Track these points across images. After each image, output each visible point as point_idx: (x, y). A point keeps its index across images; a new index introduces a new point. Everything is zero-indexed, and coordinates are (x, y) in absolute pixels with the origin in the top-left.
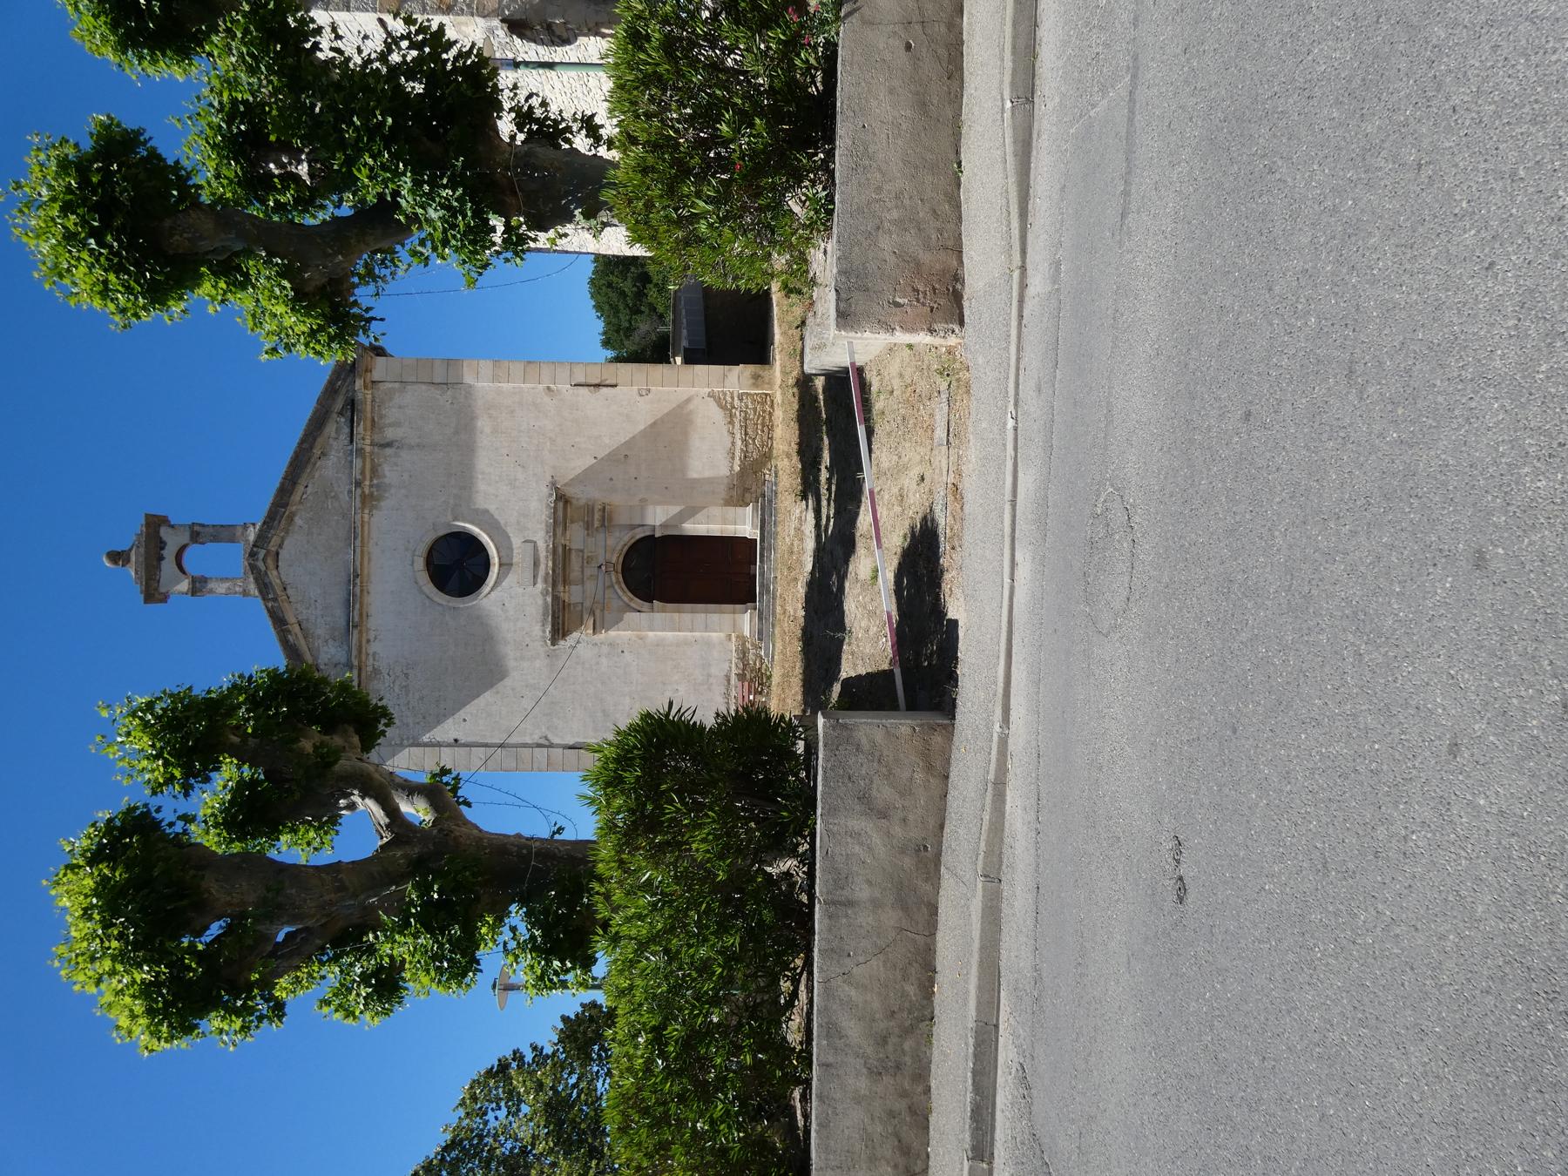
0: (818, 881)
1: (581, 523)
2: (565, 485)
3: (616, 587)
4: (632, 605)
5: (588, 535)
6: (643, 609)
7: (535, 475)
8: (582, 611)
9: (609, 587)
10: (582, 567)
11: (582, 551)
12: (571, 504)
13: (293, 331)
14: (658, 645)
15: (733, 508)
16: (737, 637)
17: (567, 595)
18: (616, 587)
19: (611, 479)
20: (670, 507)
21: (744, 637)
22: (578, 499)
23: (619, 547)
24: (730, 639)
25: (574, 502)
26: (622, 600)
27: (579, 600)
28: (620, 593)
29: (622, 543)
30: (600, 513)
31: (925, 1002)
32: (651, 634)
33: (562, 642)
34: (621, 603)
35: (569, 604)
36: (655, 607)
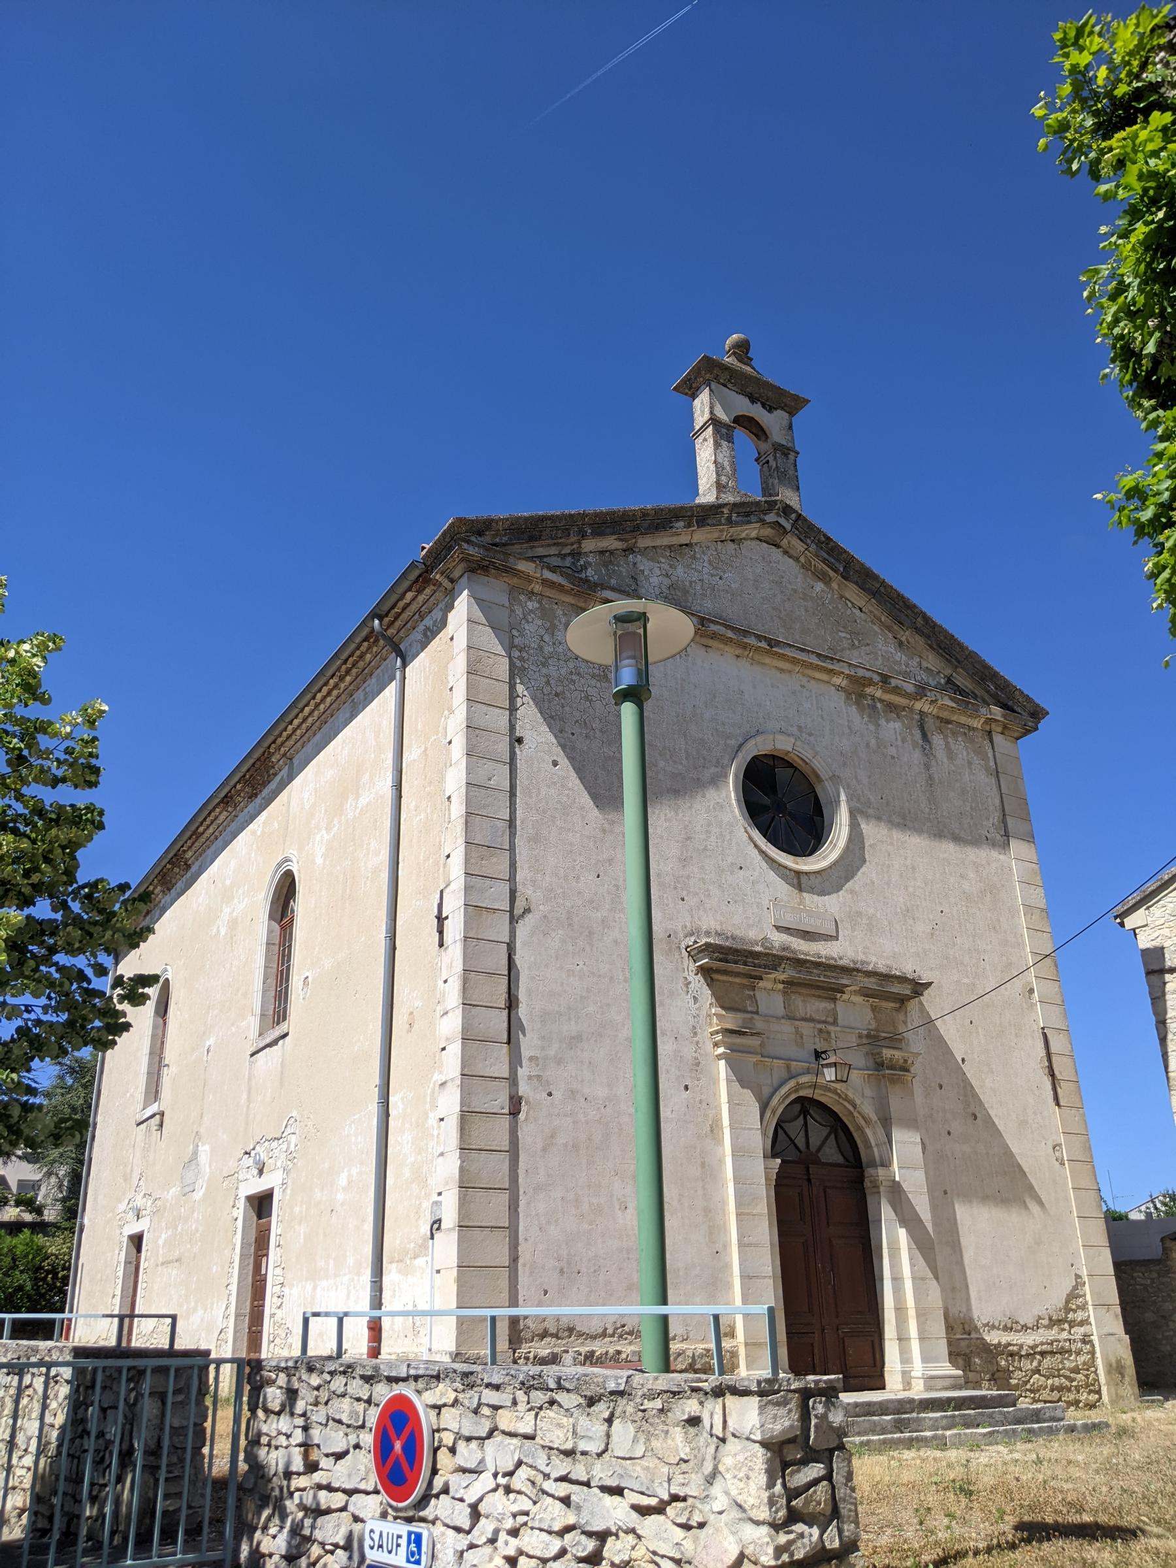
3: (792, 1083)
5: (860, 1036)
12: (898, 1010)
14: (703, 1165)
29: (858, 1102)
35: (753, 988)
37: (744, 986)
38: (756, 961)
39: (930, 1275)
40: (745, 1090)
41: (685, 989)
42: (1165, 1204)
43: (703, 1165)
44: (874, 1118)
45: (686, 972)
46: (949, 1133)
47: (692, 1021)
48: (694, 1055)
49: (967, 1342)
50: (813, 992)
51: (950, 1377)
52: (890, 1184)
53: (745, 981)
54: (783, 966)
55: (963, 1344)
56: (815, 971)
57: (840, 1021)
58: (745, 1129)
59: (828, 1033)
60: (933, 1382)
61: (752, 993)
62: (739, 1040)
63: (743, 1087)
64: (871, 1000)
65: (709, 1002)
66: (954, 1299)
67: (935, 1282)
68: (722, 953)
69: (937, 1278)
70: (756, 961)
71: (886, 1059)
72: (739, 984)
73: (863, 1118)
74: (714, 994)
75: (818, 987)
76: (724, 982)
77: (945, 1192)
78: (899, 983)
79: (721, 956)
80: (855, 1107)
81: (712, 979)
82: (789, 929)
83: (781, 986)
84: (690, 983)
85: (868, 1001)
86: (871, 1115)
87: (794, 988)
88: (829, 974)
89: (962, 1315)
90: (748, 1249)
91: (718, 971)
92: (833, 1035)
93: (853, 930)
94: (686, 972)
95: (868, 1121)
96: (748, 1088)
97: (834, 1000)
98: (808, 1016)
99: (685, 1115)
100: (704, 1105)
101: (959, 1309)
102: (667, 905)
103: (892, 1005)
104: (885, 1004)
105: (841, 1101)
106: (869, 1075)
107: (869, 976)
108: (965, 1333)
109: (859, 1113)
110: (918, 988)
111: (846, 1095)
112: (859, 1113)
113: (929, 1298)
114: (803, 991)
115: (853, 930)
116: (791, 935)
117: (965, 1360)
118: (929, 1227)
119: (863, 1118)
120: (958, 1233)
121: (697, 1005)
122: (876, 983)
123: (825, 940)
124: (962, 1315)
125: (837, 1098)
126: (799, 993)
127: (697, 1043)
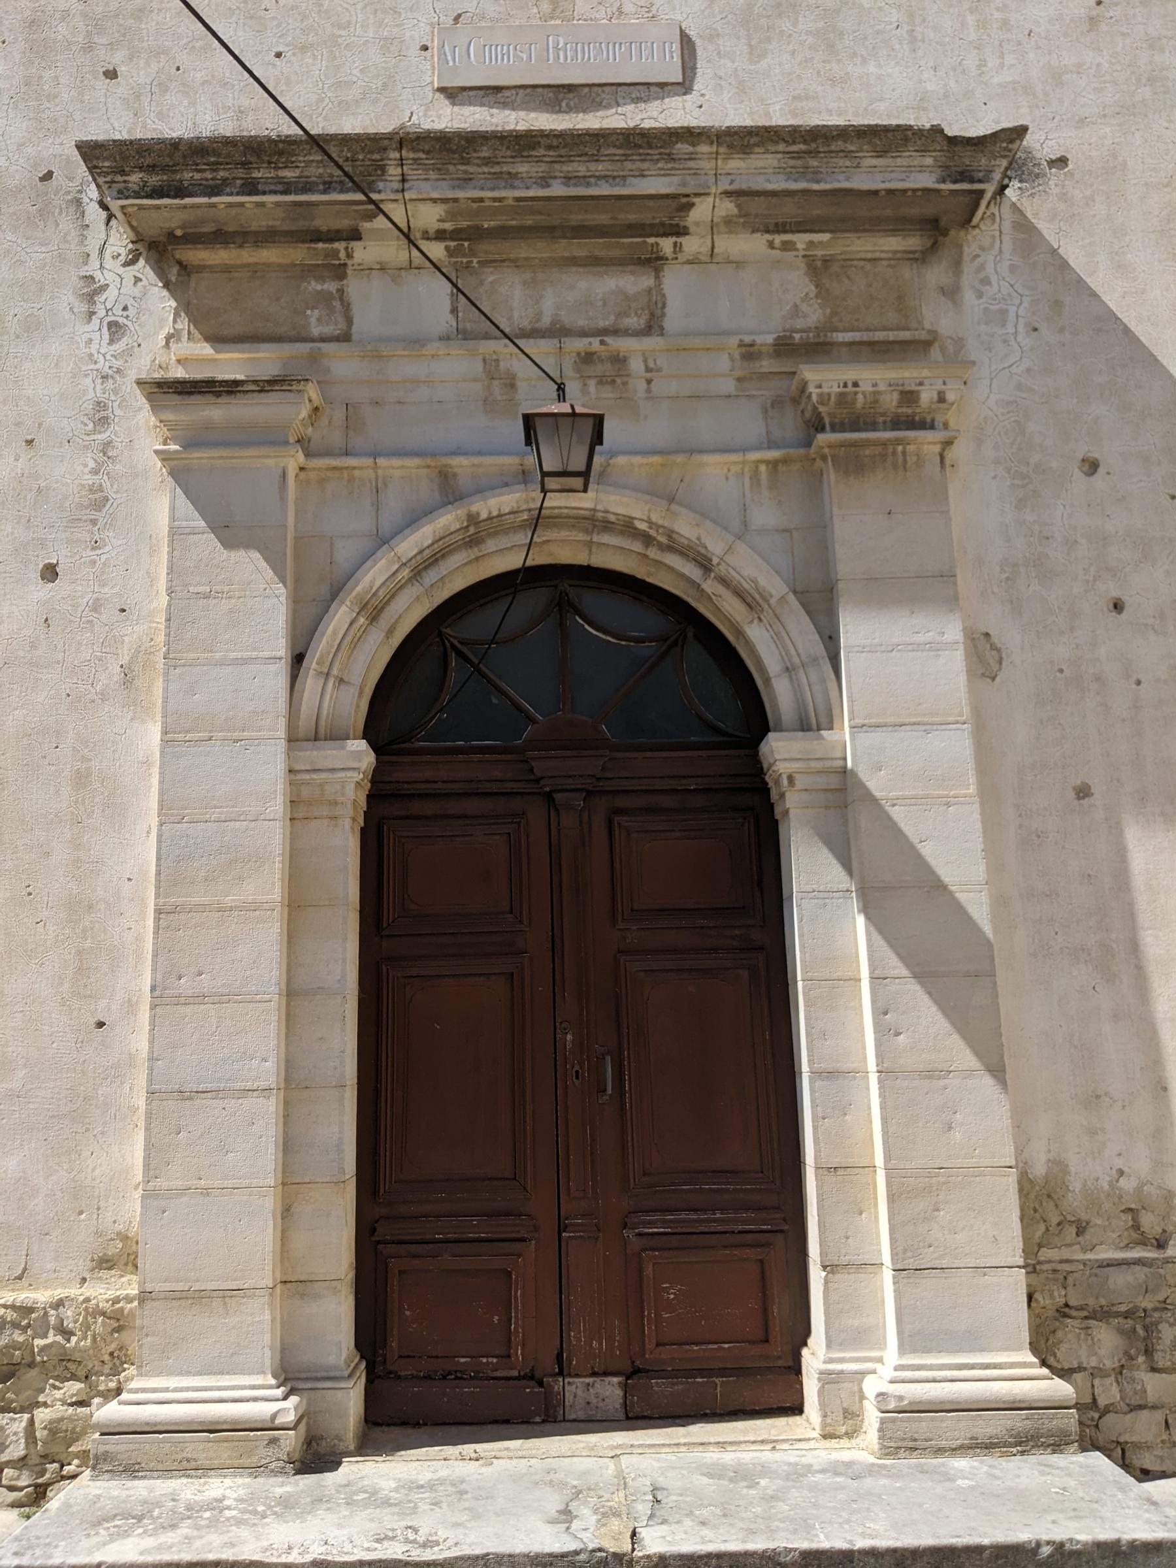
0: (327, 245)
1: (814, 315)
2: (1024, 226)
3: (448, 520)
4: (340, 617)
5: (750, 352)
6: (310, 683)
7: (1057, 77)
8: (304, 339)
9: (445, 479)
10: (558, 331)
11: (653, 326)
12: (921, 258)
13: (82, 422)
14: (81, 779)
15: (1012, 1249)
16: (118, 1321)
17: (394, 252)
18: (448, 520)
19: (1091, 466)
20: (972, 816)
21: (119, 1361)
22: (951, 293)
23: (686, 528)
24: (105, 1263)
25: (936, 274)
26: (367, 557)
27: (366, 321)
28: (410, 545)
29: (715, 547)
30: (890, 402)
31: (67, 1304)
32: (152, 734)
33: (120, 241)
34: (346, 552)
35: (340, 272)
36: (327, 755)
37: (307, 271)
38: (289, 174)
39: (967, 1059)
40: (239, 555)
41: (84, 307)
42: (148, 64)
43: (81, 779)
44: (774, 586)
45: (94, 263)
46: (1118, 606)
47: (92, 389)
48: (89, 479)
49: (1140, 1273)
50: (580, 248)
51: (1013, 1406)
52: (834, 781)
53: (298, 254)
54: (394, 171)
55: (1121, 1280)
56: (522, 168)
57: (673, 320)
58: (221, 663)
59: (619, 360)
60: (924, 1425)
61: (331, 286)
62: (216, 412)
63: (228, 544)
64: (801, 240)
65: (168, 329)
66: (1092, 1132)
67: (987, 1083)
68: (151, 168)
69: (997, 1071)
70: (289, 174)
71: (824, 399)
72: (282, 268)
73: (739, 594)
74: (186, 307)
75: (581, 231)
76: (227, 269)
77: (1083, 792)
78: (881, 153)
79: (154, 180)
80: (705, 565)
81: (183, 267)
82: (498, 89)
83: (437, 250)
84: (104, 288)
85: (788, 246)
86: (762, 582)
87: (488, 248)
88: (581, 169)
89: (1127, 1184)
90: (189, 1009)
91: (193, 239)
92: (636, 365)
93: (756, 53)
94: (94, 263)
95: (752, 602)
96: (247, 547)
97: (654, 262)
98: (546, 321)
99: (33, 646)
100: (109, 614)
101: (1119, 1163)
102: (52, 97)
103: (893, 243)
104: (861, 245)
105: (653, 553)
106: (774, 465)
107: (746, 150)
108: (1143, 1242)
109: (724, 581)
110: (966, 158)
111: (670, 534)
112: (724, 581)
113: (957, 1135)
114: (523, 250)
115: (756, 53)
116: (505, 105)
117: (1130, 1334)
118: (978, 907)
119: (739, 594)
120: (1130, 915)
121: (120, 346)
122: (779, 170)
123: (637, 100)
124: (1127, 1184)
125: (637, 546)
126: (516, 264)
127: (106, 446)
